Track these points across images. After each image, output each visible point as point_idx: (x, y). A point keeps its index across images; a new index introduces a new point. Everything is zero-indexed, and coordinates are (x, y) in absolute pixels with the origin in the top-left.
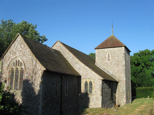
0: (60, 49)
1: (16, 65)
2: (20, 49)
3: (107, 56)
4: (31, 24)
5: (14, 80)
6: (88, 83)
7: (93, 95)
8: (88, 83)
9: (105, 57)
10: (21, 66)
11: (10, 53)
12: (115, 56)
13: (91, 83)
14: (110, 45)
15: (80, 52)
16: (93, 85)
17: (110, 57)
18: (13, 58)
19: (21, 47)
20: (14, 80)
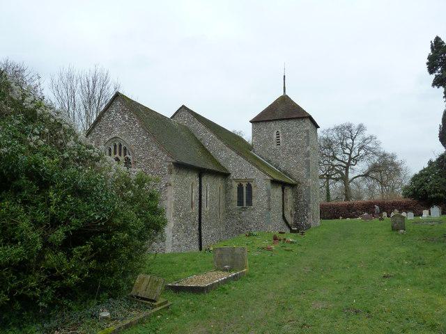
0: (188, 122)
1: (125, 154)
2: (123, 121)
3: (275, 136)
4: (361, 128)
5: (245, 201)
6: (244, 185)
7: (254, 209)
8: (244, 185)
9: (271, 139)
10: (125, 154)
11: (101, 130)
12: (290, 136)
13: (249, 187)
14: (308, 121)
15: (152, 111)
16: (254, 190)
17: (280, 138)
18: (108, 139)
19: (124, 119)
20: (245, 201)
